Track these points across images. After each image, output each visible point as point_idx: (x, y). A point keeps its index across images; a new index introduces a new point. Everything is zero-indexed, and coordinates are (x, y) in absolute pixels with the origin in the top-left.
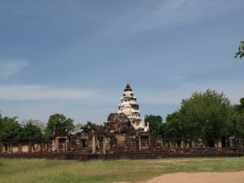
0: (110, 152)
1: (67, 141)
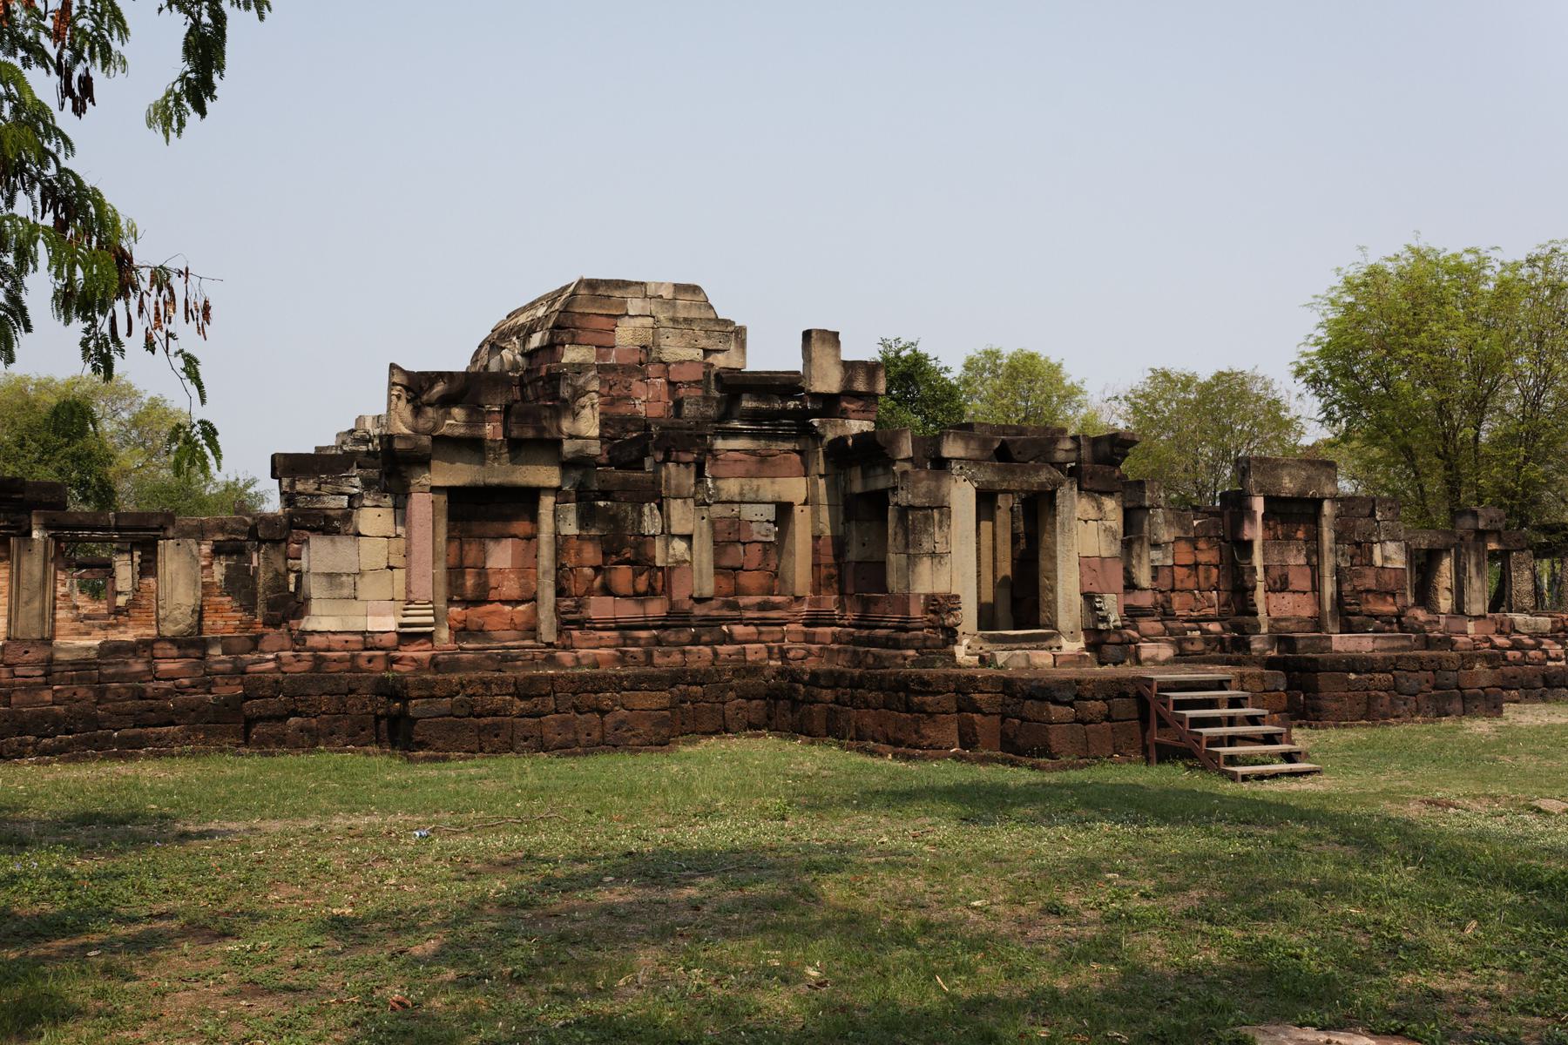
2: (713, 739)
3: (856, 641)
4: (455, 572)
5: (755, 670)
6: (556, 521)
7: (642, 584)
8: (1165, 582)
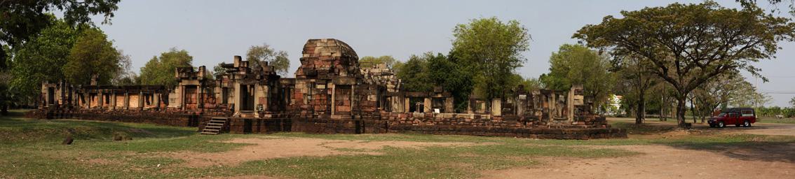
0: (266, 115)
1: (199, 91)
7: (214, 101)
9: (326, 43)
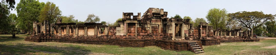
2: (150, 46)
3: (164, 37)
4: (128, 30)
5: (154, 40)
6: (137, 26)
7: (145, 32)
8: (193, 33)
9: (157, 10)
